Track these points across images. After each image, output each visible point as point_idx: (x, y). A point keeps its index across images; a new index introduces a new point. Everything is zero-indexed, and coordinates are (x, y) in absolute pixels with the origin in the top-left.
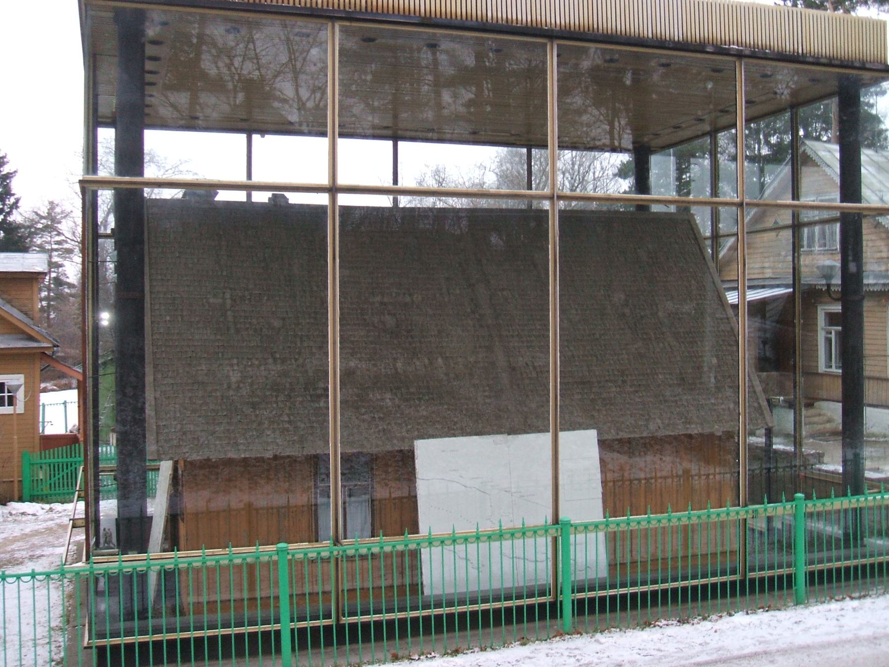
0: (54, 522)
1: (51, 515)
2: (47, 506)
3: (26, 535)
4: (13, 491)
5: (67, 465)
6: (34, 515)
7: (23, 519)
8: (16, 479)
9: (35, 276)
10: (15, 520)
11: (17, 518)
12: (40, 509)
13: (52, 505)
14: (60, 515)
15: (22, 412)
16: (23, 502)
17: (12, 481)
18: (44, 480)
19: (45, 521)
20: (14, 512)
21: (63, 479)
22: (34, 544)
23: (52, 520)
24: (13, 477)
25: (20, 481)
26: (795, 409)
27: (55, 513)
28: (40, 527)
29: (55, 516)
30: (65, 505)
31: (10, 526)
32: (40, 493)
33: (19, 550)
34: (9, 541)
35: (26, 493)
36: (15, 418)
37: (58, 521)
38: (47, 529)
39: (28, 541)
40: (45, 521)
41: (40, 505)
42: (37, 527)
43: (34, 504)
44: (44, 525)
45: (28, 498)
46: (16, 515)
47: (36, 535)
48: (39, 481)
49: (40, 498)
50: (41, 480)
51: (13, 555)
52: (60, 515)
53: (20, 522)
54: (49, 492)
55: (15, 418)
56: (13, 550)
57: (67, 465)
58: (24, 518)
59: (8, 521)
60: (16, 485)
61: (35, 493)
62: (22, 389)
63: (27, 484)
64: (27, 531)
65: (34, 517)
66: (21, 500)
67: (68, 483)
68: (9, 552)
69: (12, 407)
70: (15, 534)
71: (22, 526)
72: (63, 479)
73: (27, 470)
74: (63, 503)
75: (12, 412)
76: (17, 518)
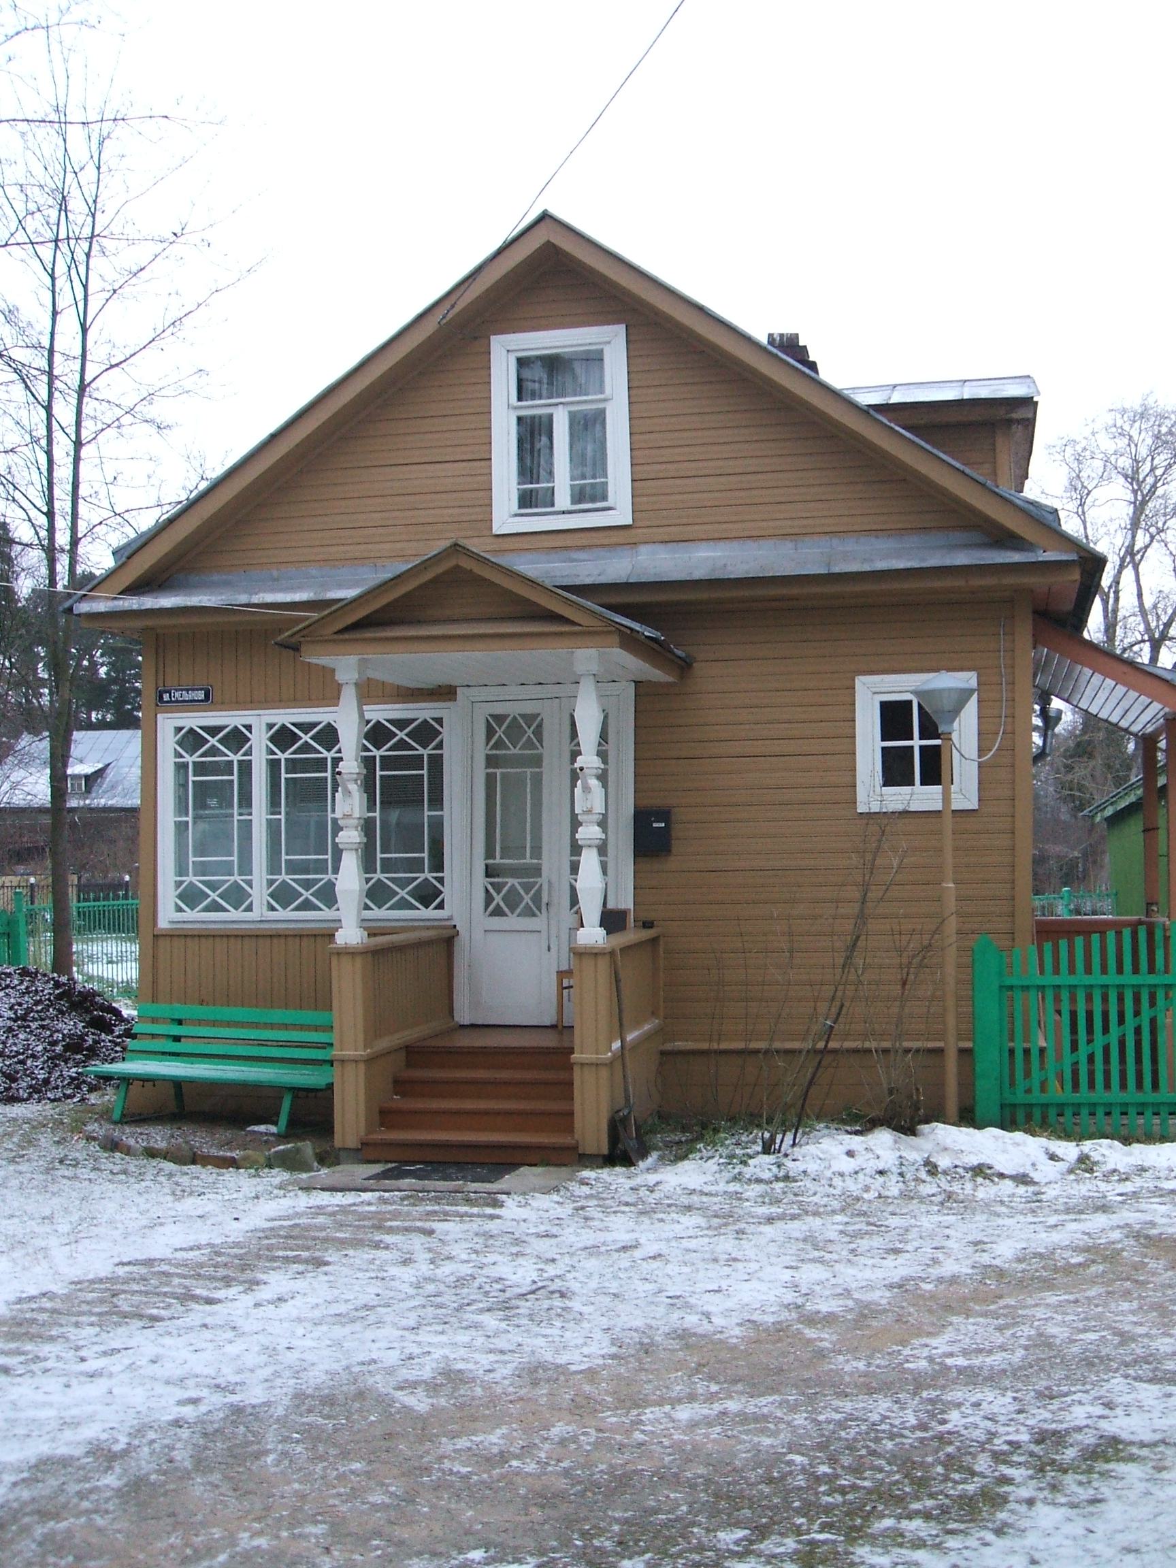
0: (1116, 1219)
1: (1085, 1188)
2: (1069, 1150)
3: (1000, 1273)
4: (941, 1084)
5: (1137, 1000)
6: (1022, 1179)
7: (981, 1194)
8: (952, 1047)
9: (1001, 413)
10: (950, 1196)
11: (956, 1187)
12: (1043, 1158)
13: (1087, 1146)
14: (1128, 1187)
15: (973, 804)
16: (979, 1126)
17: (939, 1052)
18: (1051, 1055)
19: (1076, 1210)
20: (944, 1162)
21: (1107, 1060)
22: (1043, 1341)
23: (1104, 1208)
24: (942, 1036)
25: (965, 1053)
26: (358, 1150)
27: (1106, 1177)
28: (1056, 1237)
29: (1112, 1191)
30: (1136, 1147)
31: (928, 1221)
32: (1036, 1097)
33: (970, 1377)
34: (919, 1299)
35: (987, 1093)
36: (948, 820)
37: (1128, 1216)
38: (1096, 1252)
39: (1013, 1319)
40: (1076, 1210)
41: (1042, 1141)
42: (1044, 1240)
43: (1019, 1136)
44: (1072, 1232)
45: (995, 1111)
46: (952, 1173)
47: (1048, 1284)
48: (1035, 1054)
49: (1037, 1114)
50: (1042, 1051)
51: (937, 1409)
52: (1128, 1187)
53: (967, 1206)
54: (1068, 1096)
55: (948, 822)
56: (941, 1375)
57: (1137, 1000)
58: (986, 1191)
59: (922, 1200)
60: (951, 1062)
61: (1020, 1097)
62: (971, 709)
63: (989, 1061)
64: (1004, 1251)
65: (1022, 1189)
66: (968, 1117)
67: (1107, 1074)
68: (919, 1383)
69: (938, 789)
70: (949, 1268)
71: (977, 1226)
72: (1107, 1060)
73: (989, 1010)
74: (1126, 1141)
75: (938, 806)
76: (956, 1187)
